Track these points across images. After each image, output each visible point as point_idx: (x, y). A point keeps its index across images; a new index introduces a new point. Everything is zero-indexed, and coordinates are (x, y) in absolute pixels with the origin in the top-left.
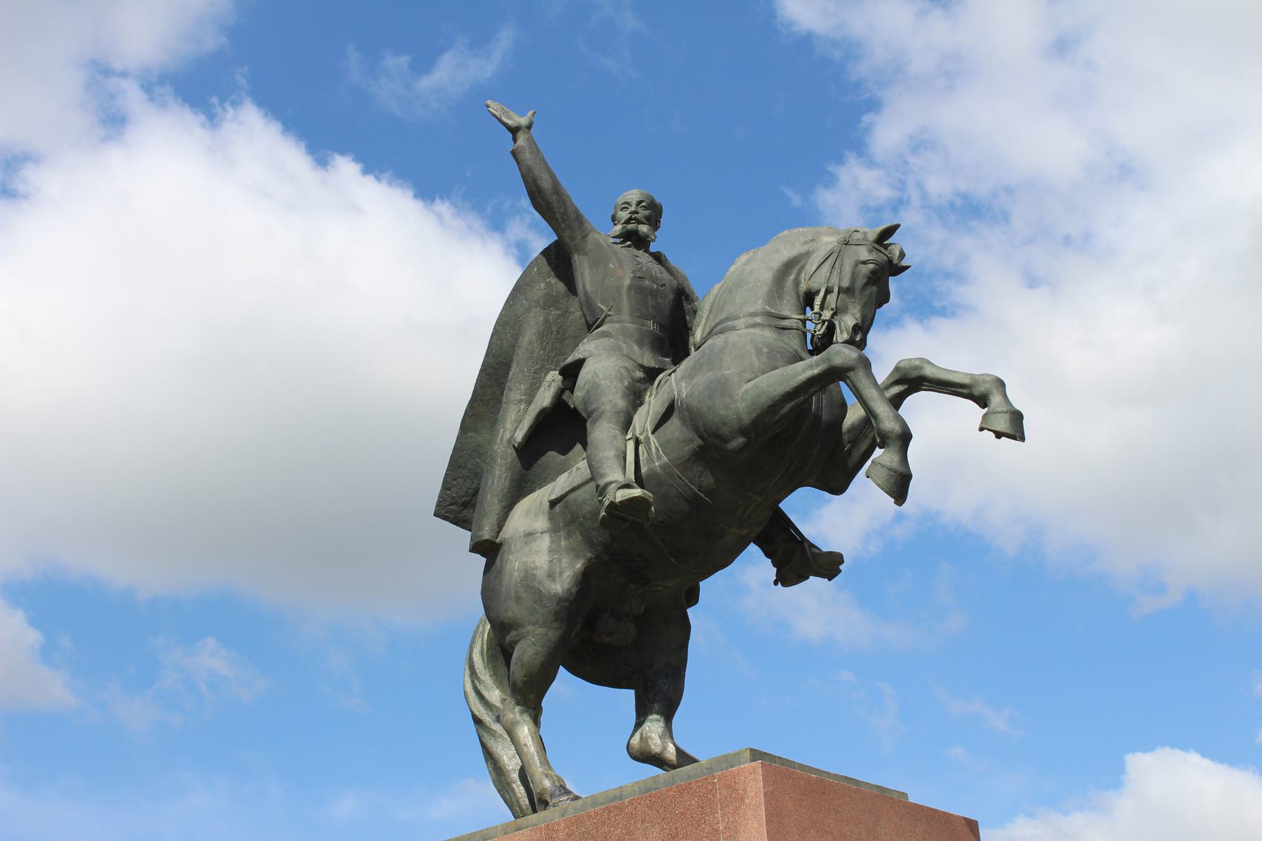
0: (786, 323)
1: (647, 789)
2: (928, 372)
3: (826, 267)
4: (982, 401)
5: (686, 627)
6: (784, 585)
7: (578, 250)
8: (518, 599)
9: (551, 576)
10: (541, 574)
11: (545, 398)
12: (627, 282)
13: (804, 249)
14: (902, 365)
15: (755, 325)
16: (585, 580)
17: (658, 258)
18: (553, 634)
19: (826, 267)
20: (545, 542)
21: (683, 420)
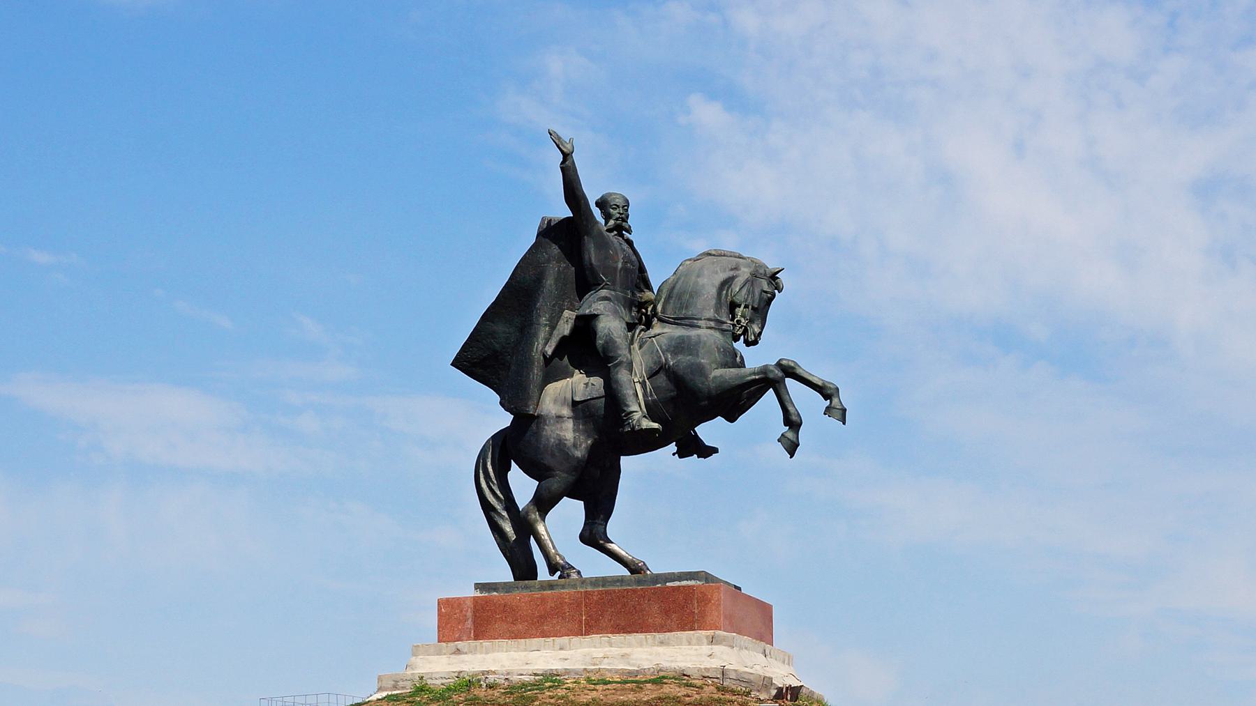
0: (724, 327)
1: (620, 580)
2: (799, 371)
3: (744, 291)
4: (827, 397)
5: (617, 470)
6: (681, 457)
7: (588, 234)
8: (553, 455)
9: (575, 445)
10: (570, 443)
11: (565, 328)
12: (620, 265)
13: (731, 273)
14: (784, 362)
15: (711, 328)
16: (592, 450)
17: (630, 243)
18: (571, 479)
19: (744, 291)
20: (570, 424)
21: (668, 377)
